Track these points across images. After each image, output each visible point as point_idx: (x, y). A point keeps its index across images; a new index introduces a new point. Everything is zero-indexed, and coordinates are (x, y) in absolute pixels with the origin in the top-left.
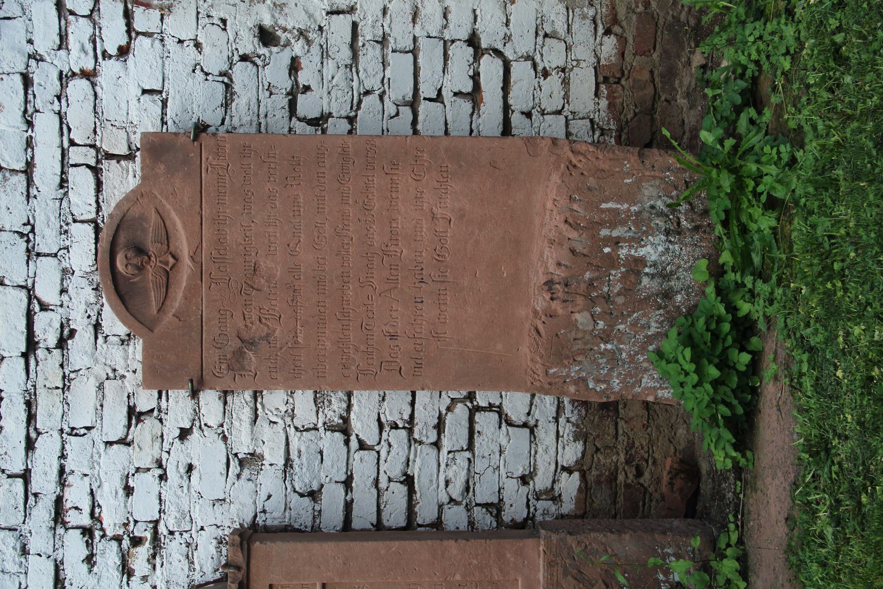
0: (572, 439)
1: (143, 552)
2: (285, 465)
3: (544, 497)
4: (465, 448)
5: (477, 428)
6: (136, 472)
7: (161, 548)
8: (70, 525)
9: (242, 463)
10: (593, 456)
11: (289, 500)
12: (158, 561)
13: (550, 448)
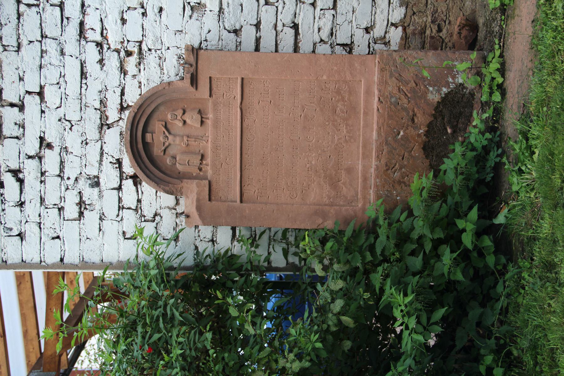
0: (398, 5)
1: (132, 61)
2: (219, 12)
3: (379, 42)
4: (331, 8)
6: (128, 10)
7: (143, 59)
8: (88, 40)
9: (192, 8)
10: (411, 17)
11: (221, 34)
12: (142, 67)
13: (384, 10)
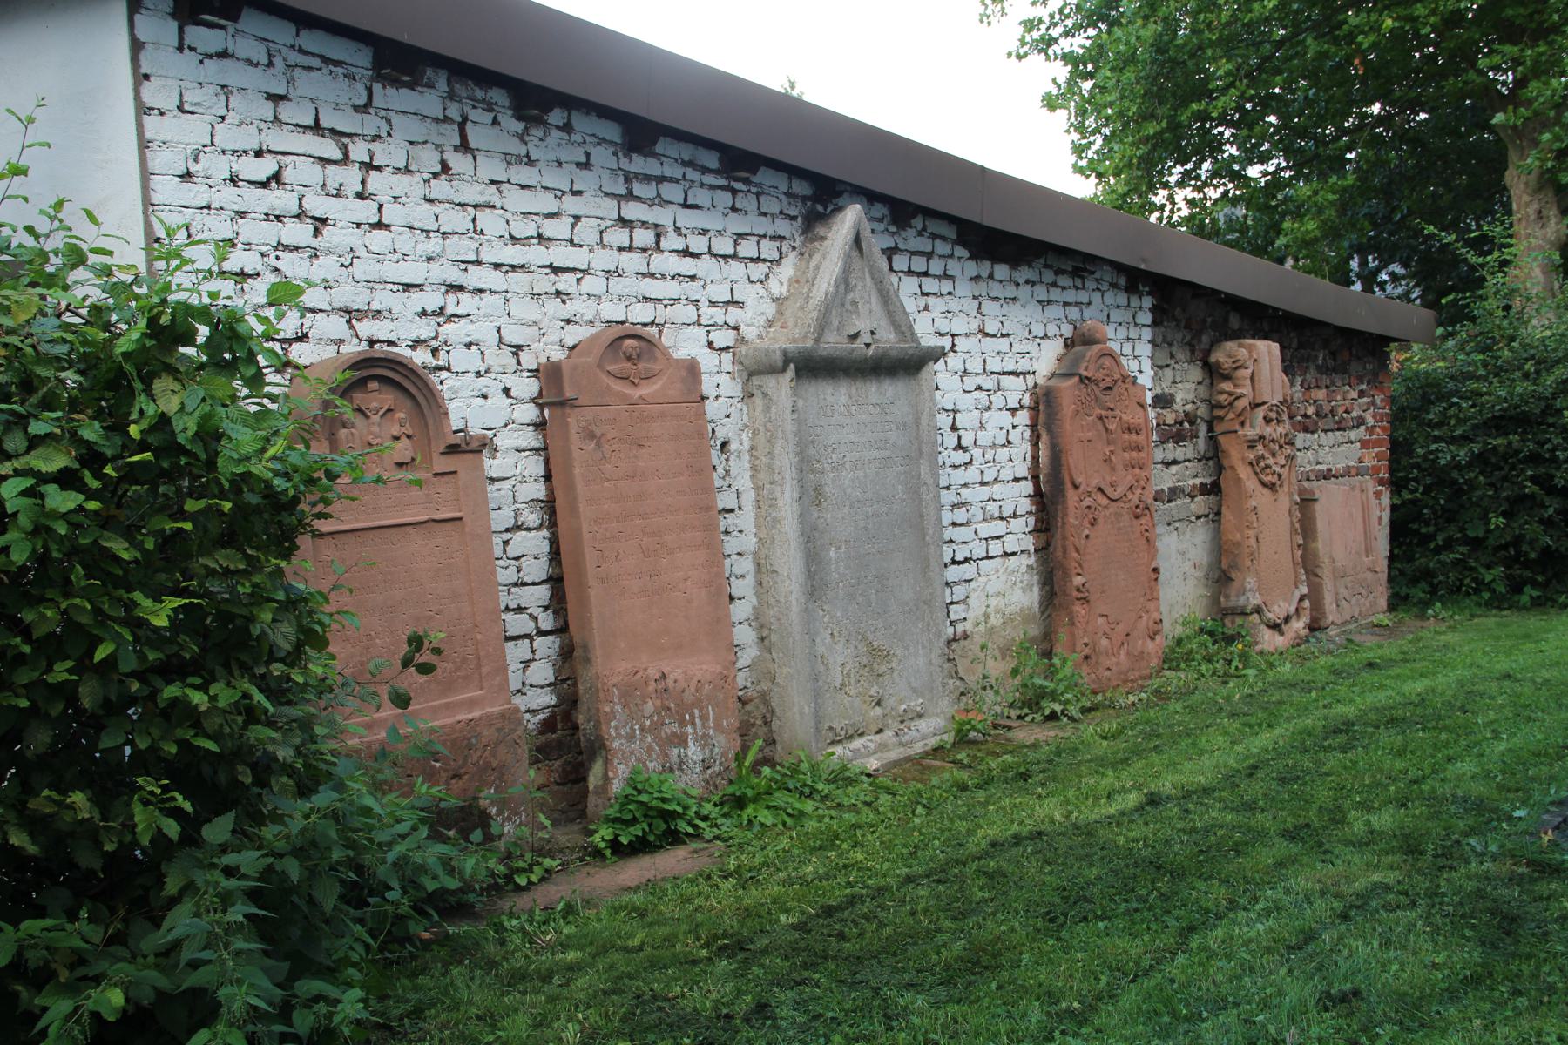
5: (520, 642)
